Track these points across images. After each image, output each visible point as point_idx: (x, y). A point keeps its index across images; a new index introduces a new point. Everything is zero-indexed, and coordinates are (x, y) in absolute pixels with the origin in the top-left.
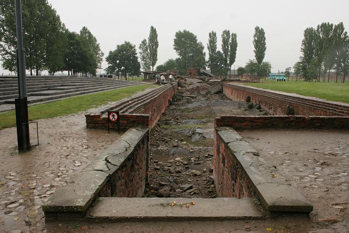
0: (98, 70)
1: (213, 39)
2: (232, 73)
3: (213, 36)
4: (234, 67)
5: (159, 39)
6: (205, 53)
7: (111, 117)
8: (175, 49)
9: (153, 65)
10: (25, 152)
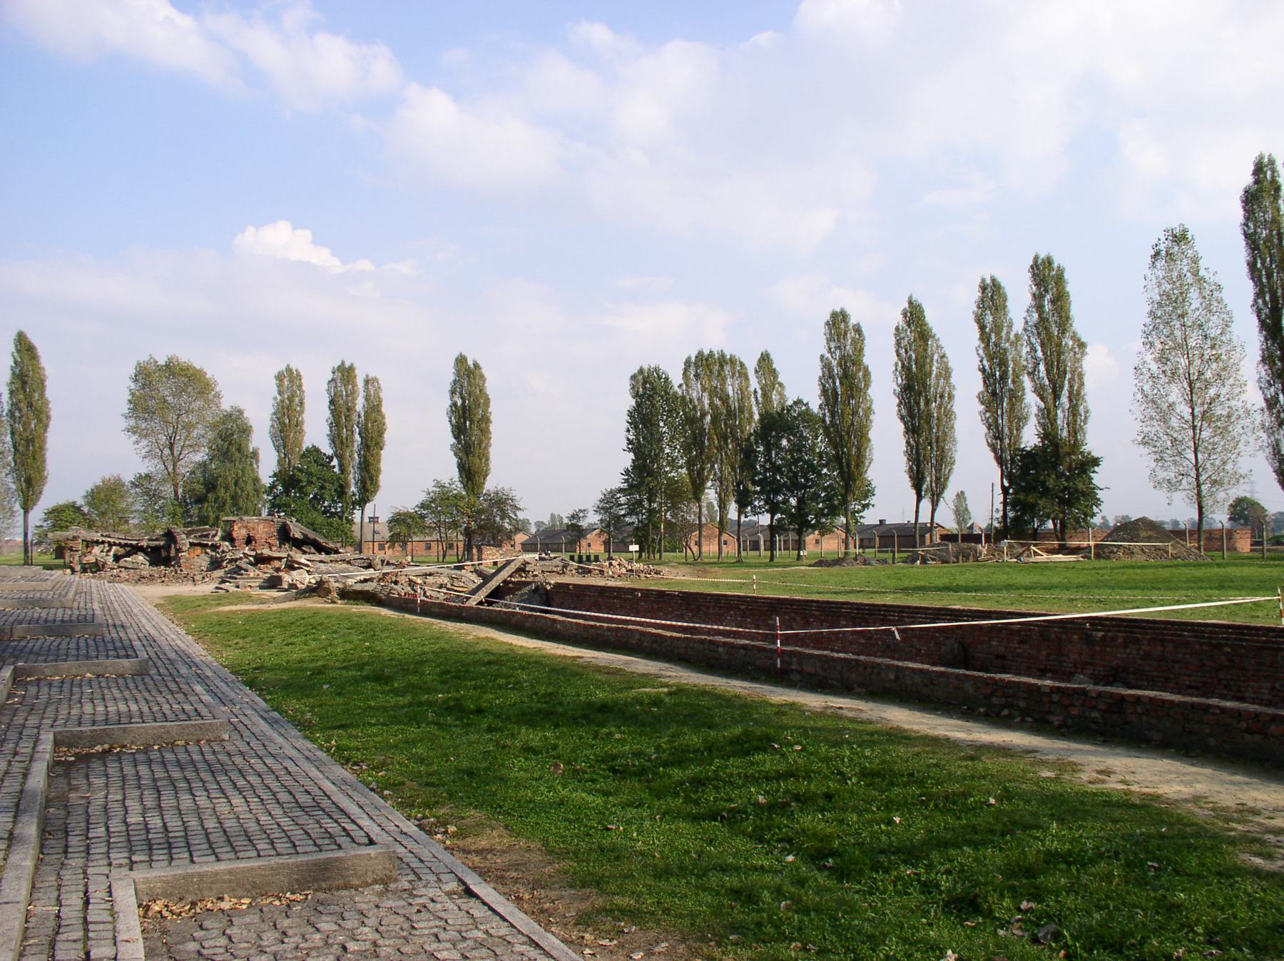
1: (291, 399)
3: (289, 381)
4: (384, 505)
5: (1082, 318)
6: (255, 454)
8: (132, 430)
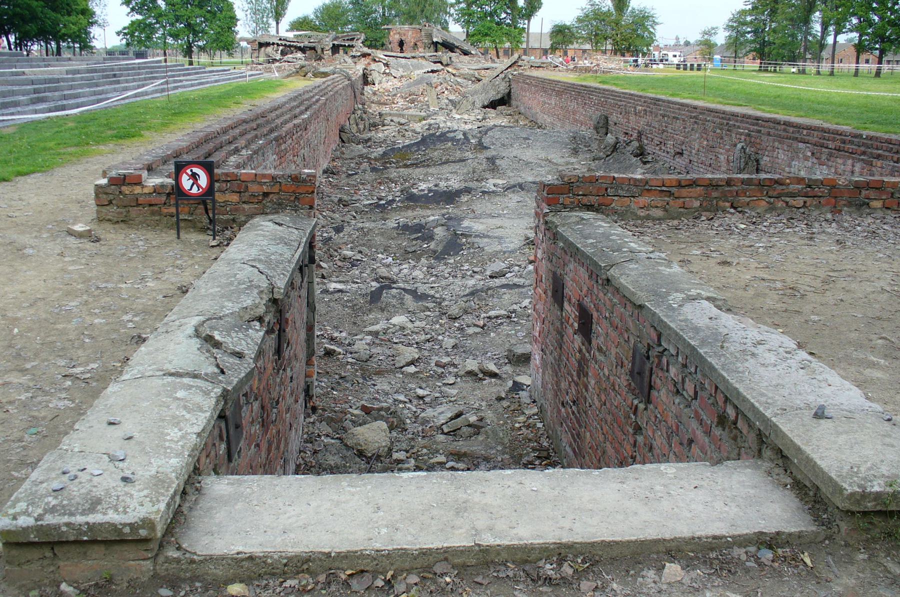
0: (95, 31)
2: (534, 44)
7: (186, 182)
9: (278, 16)
10: (296, 556)
